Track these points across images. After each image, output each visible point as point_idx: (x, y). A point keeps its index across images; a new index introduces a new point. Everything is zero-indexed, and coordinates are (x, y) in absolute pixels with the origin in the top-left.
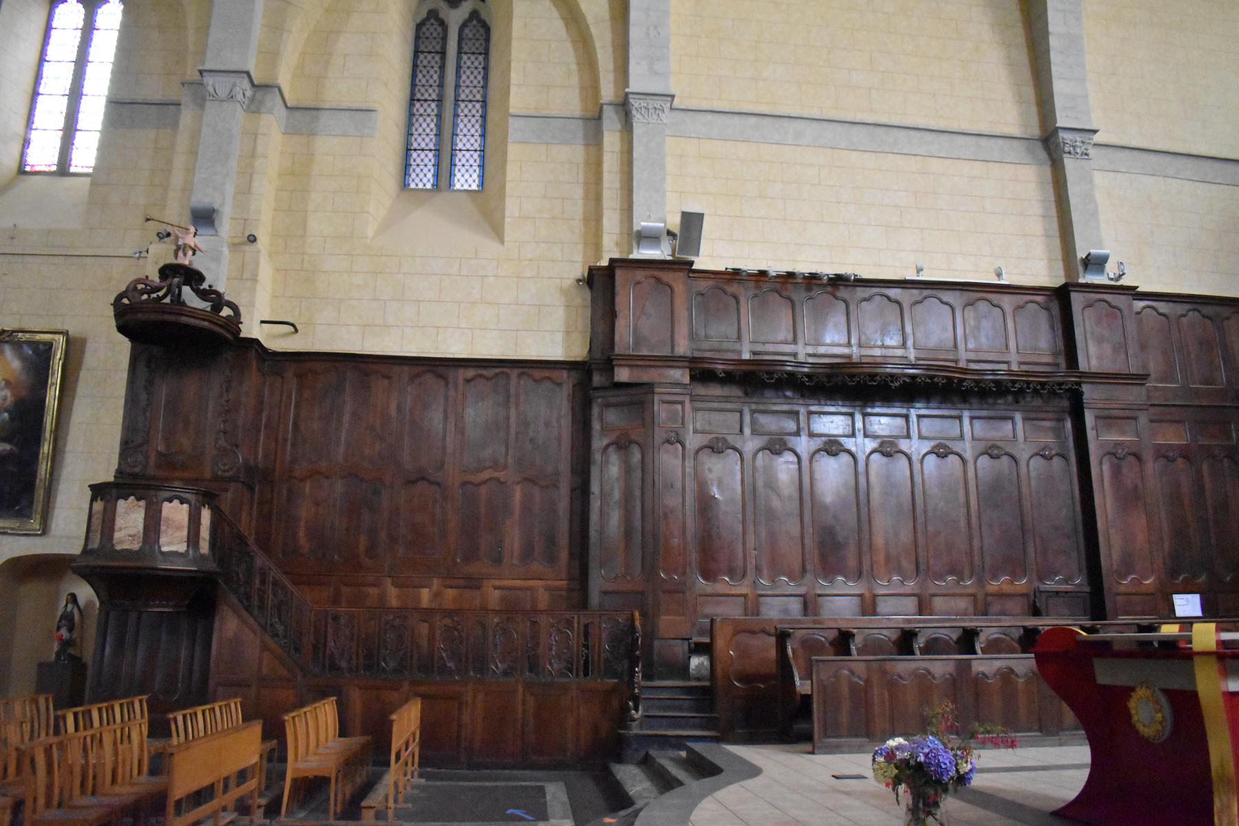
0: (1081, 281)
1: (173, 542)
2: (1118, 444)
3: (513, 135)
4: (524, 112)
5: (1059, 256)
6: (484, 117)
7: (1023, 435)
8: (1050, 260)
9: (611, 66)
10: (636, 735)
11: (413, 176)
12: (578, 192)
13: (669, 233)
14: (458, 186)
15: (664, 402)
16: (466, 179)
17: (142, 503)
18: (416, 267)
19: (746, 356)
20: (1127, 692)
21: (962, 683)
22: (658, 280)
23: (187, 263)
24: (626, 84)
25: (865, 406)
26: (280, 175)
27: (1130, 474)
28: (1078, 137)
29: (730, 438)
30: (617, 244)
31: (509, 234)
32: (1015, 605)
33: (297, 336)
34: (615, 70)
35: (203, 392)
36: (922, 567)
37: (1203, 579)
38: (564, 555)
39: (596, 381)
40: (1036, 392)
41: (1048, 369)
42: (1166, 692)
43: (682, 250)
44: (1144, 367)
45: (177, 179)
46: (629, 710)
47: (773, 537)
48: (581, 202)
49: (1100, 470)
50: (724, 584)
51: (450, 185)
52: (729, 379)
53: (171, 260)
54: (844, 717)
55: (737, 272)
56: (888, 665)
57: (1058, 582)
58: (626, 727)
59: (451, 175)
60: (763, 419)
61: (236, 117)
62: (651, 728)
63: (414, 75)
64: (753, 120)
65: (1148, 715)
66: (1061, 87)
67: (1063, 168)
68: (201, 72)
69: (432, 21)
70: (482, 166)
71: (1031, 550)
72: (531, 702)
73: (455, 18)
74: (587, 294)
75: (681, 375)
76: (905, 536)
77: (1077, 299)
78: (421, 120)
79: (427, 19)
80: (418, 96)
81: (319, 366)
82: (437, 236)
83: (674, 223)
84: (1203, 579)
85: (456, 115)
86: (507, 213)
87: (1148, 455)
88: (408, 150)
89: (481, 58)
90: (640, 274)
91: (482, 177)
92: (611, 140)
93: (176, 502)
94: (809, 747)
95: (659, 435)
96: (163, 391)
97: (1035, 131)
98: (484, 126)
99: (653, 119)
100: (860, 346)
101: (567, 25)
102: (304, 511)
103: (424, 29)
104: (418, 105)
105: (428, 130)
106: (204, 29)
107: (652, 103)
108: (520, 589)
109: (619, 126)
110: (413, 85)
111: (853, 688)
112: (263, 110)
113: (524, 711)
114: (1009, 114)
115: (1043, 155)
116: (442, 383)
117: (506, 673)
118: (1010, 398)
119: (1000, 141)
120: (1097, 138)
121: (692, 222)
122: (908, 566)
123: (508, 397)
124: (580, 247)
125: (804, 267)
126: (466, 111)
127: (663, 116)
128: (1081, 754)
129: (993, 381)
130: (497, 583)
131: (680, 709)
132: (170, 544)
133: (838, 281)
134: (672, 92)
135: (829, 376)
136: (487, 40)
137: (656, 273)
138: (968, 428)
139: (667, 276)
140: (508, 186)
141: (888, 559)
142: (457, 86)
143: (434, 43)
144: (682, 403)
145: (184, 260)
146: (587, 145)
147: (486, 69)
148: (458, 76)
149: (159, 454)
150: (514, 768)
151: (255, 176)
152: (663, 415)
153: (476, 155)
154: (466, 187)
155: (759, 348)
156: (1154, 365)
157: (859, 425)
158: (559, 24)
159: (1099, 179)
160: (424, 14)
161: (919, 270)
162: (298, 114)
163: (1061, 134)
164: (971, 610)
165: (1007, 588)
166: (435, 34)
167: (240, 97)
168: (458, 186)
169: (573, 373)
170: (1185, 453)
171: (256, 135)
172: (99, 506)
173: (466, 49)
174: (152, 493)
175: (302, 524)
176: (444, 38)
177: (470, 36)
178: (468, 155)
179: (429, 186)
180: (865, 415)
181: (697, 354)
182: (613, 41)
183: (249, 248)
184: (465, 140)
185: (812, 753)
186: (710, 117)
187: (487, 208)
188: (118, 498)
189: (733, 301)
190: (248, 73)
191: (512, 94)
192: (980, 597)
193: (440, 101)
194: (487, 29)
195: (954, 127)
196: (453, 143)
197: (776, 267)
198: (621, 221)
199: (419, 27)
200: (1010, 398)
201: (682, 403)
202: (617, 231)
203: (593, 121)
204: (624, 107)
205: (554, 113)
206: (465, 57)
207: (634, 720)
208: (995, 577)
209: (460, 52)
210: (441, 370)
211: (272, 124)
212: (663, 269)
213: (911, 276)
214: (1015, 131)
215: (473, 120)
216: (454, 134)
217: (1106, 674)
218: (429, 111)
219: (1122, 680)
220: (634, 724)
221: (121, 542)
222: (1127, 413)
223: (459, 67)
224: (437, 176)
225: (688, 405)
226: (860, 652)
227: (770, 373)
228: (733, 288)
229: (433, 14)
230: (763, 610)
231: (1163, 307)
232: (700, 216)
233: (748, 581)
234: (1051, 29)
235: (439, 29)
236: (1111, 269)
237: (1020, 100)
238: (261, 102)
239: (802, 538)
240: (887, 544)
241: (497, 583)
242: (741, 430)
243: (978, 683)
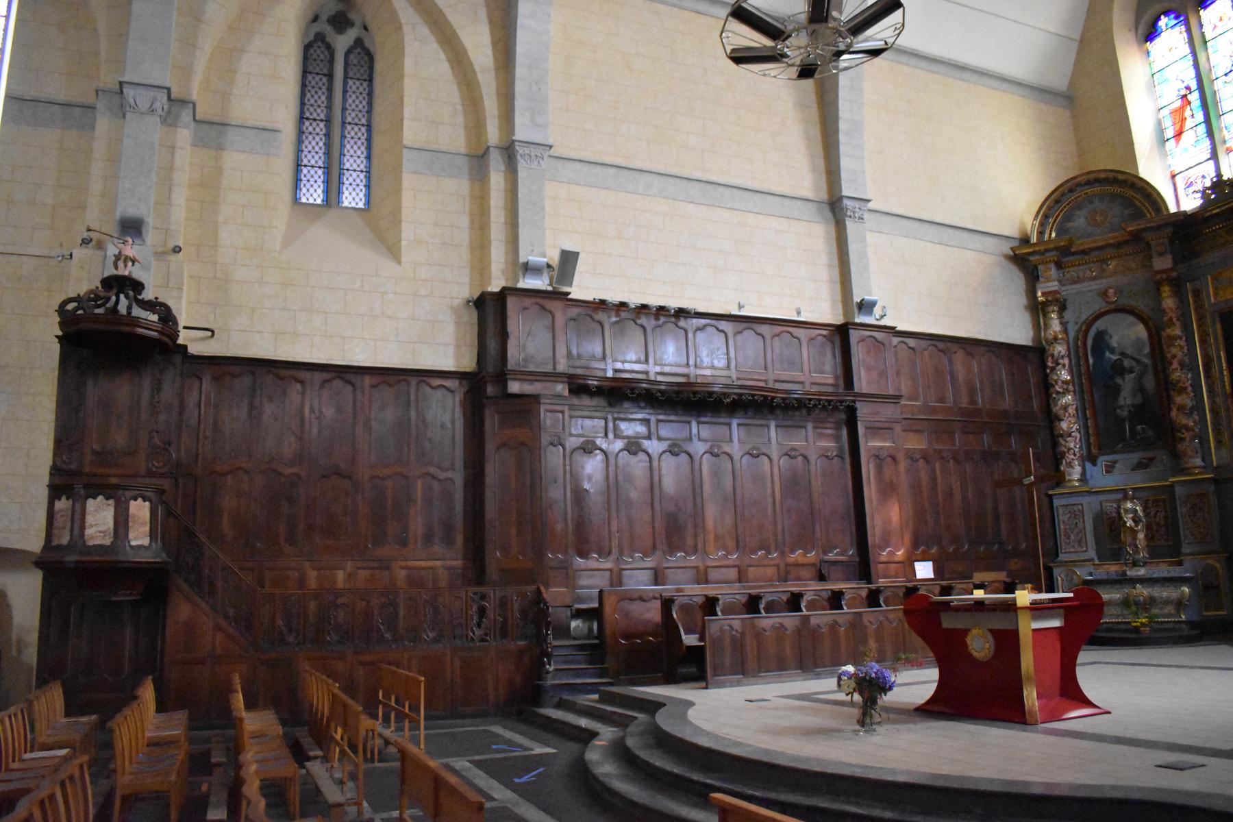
0: (857, 320)
1: (139, 536)
2: (881, 448)
3: (406, 165)
4: (417, 145)
5: (839, 298)
6: (369, 140)
7: (816, 443)
8: (833, 301)
9: (496, 113)
10: (553, 685)
11: (304, 190)
12: (465, 222)
13: (549, 266)
14: (346, 204)
15: (550, 411)
16: (353, 197)
17: (111, 502)
18: (331, 288)
19: (610, 374)
20: (966, 632)
21: (806, 633)
22: (543, 307)
23: (126, 273)
24: (513, 134)
25: (699, 416)
26: (189, 185)
27: (888, 473)
28: (857, 204)
29: (598, 442)
30: (503, 272)
31: (405, 258)
32: (806, 573)
33: (212, 341)
34: (500, 116)
35: (123, 390)
36: (741, 545)
37: (934, 550)
38: (459, 539)
39: (490, 392)
40: (824, 407)
41: (830, 389)
42: (991, 631)
43: (558, 282)
44: (899, 390)
45: (96, 186)
46: (544, 665)
47: (631, 523)
48: (467, 232)
49: (868, 470)
50: (594, 562)
51: (339, 201)
52: (599, 392)
53: (110, 271)
54: (727, 661)
55: (603, 302)
56: (756, 621)
57: (837, 554)
58: (540, 679)
59: (340, 192)
60: (623, 426)
61: (152, 129)
62: (560, 678)
63: (303, 95)
64: (612, 171)
65: (980, 645)
66: (846, 163)
67: (845, 228)
68: (121, 83)
69: (320, 44)
70: (368, 187)
71: (818, 528)
72: (458, 663)
73: (342, 42)
74: (475, 314)
75: (561, 388)
76: (729, 519)
77: (854, 335)
78: (310, 138)
79: (315, 41)
80: (307, 115)
81: (237, 369)
82: (336, 254)
83: (554, 257)
84: (934, 550)
85: (343, 136)
86: (403, 235)
87: (900, 456)
88: (298, 166)
89: (365, 84)
90: (528, 302)
91: (368, 196)
92: (497, 179)
93: (140, 500)
94: (704, 684)
95: (545, 439)
96: (94, 390)
97: (824, 196)
98: (369, 148)
99: (534, 165)
100: (696, 366)
101: (452, 68)
102: (228, 502)
103: (312, 51)
104: (307, 123)
105: (317, 149)
106: (120, 38)
107: (534, 151)
108: (426, 568)
109: (503, 168)
110: (302, 104)
111: (733, 638)
112: (180, 124)
113: (452, 672)
114: (804, 180)
115: (829, 215)
116: (350, 388)
117: (435, 640)
118: (804, 412)
119: (799, 202)
120: (870, 205)
121: (569, 259)
122: (731, 544)
123: (409, 404)
124: (467, 271)
125: (654, 301)
126: (353, 134)
127: (542, 163)
128: (933, 674)
129: (795, 399)
130: (403, 563)
131: (578, 662)
132: (136, 539)
133: (681, 313)
134: (550, 142)
135: (678, 393)
136: (371, 68)
137: (541, 301)
138: (774, 436)
139: (550, 304)
140: (404, 212)
141: (717, 537)
142: (344, 109)
143: (321, 65)
144: (562, 412)
145: (123, 271)
146: (472, 180)
147: (370, 94)
148: (344, 100)
149: (95, 453)
150: (445, 718)
151: (174, 188)
152: (548, 422)
153: (362, 176)
154: (353, 205)
155: (619, 366)
156: (905, 389)
157: (695, 431)
158: (445, 66)
159: (871, 238)
160: (311, 37)
161: (740, 307)
162: (205, 127)
163: (846, 202)
164: (776, 577)
165: (801, 560)
166: (322, 56)
167: (159, 111)
168: (346, 204)
169: (464, 382)
170: (925, 456)
171: (173, 148)
172: (62, 504)
173: (351, 74)
174: (121, 492)
175: (226, 515)
176: (332, 61)
177: (355, 62)
178: (355, 175)
179: (319, 201)
180: (698, 423)
181: (572, 371)
182: (498, 90)
183: (173, 258)
184: (351, 161)
185: (706, 688)
186: (578, 165)
187: (380, 226)
188: (87, 498)
189: (598, 326)
190: (169, 89)
191: (405, 127)
192: (782, 566)
193: (328, 121)
194: (370, 57)
195: (765, 188)
196: (341, 163)
197: (635, 300)
198: (506, 253)
199: (307, 48)
200: (804, 412)
201: (562, 412)
202: (503, 260)
203: (478, 160)
204: (509, 151)
205: (443, 148)
206: (350, 82)
207: (548, 672)
208: (793, 552)
209: (346, 77)
210: (349, 376)
211: (184, 135)
212: (550, 298)
213: (735, 311)
214: (809, 194)
215: (359, 143)
216: (342, 155)
217: (948, 622)
218: (318, 130)
219: (959, 625)
220: (549, 676)
221: (92, 538)
222: (887, 425)
223: (345, 92)
224: (327, 192)
225: (567, 414)
226: (724, 613)
227: (632, 390)
228: (600, 316)
229: (320, 37)
230: (625, 580)
231: (912, 342)
232: (575, 255)
233: (612, 558)
234: (841, 114)
235: (326, 53)
236: (877, 311)
237: (814, 169)
238: (177, 117)
239: (653, 522)
240: (715, 527)
241: (403, 563)
242: (606, 435)
243: (815, 634)
